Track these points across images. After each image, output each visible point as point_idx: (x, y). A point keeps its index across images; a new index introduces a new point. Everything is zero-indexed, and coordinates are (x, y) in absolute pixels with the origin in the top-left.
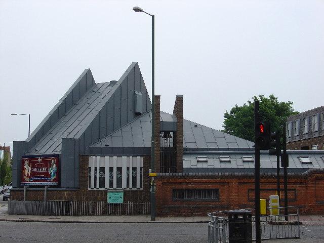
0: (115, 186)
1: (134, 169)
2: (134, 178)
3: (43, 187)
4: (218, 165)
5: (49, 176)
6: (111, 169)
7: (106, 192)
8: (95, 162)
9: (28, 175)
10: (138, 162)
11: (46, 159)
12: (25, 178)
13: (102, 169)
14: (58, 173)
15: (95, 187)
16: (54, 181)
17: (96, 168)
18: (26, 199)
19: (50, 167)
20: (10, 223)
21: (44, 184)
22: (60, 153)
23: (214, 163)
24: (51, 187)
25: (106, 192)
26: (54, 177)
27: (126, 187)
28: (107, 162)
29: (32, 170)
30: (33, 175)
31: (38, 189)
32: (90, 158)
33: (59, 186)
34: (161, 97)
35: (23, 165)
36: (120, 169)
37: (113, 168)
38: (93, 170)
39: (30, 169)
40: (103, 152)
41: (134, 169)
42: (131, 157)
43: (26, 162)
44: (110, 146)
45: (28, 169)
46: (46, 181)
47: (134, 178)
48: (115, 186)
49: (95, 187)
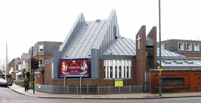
0: (118, 77)
1: (128, 67)
2: (128, 73)
3: (79, 77)
4: (176, 65)
5: (82, 71)
6: (116, 67)
7: (114, 80)
8: (108, 63)
9: (65, 71)
10: (129, 63)
11: (79, 62)
12: (63, 72)
13: (111, 67)
14: (89, 70)
15: (108, 78)
16: (85, 74)
17: (124, 67)
18: (159, 87)
19: (82, 66)
20: (195, 98)
21: (79, 76)
22: (90, 57)
23: (173, 64)
24: (83, 77)
25: (114, 80)
26: (86, 72)
27: (115, 78)
28: (114, 63)
29: (68, 68)
30: (68, 70)
31: (72, 79)
32: (104, 61)
33: (90, 77)
34: (84, 15)
35: (61, 65)
36: (120, 67)
37: (118, 68)
38: (106, 68)
39: (67, 67)
40: (112, 57)
41: (128, 67)
42: (126, 61)
43: (64, 63)
44: (112, 54)
45: (64, 67)
46: (79, 74)
47: (128, 73)
48: (118, 77)
49: (108, 78)
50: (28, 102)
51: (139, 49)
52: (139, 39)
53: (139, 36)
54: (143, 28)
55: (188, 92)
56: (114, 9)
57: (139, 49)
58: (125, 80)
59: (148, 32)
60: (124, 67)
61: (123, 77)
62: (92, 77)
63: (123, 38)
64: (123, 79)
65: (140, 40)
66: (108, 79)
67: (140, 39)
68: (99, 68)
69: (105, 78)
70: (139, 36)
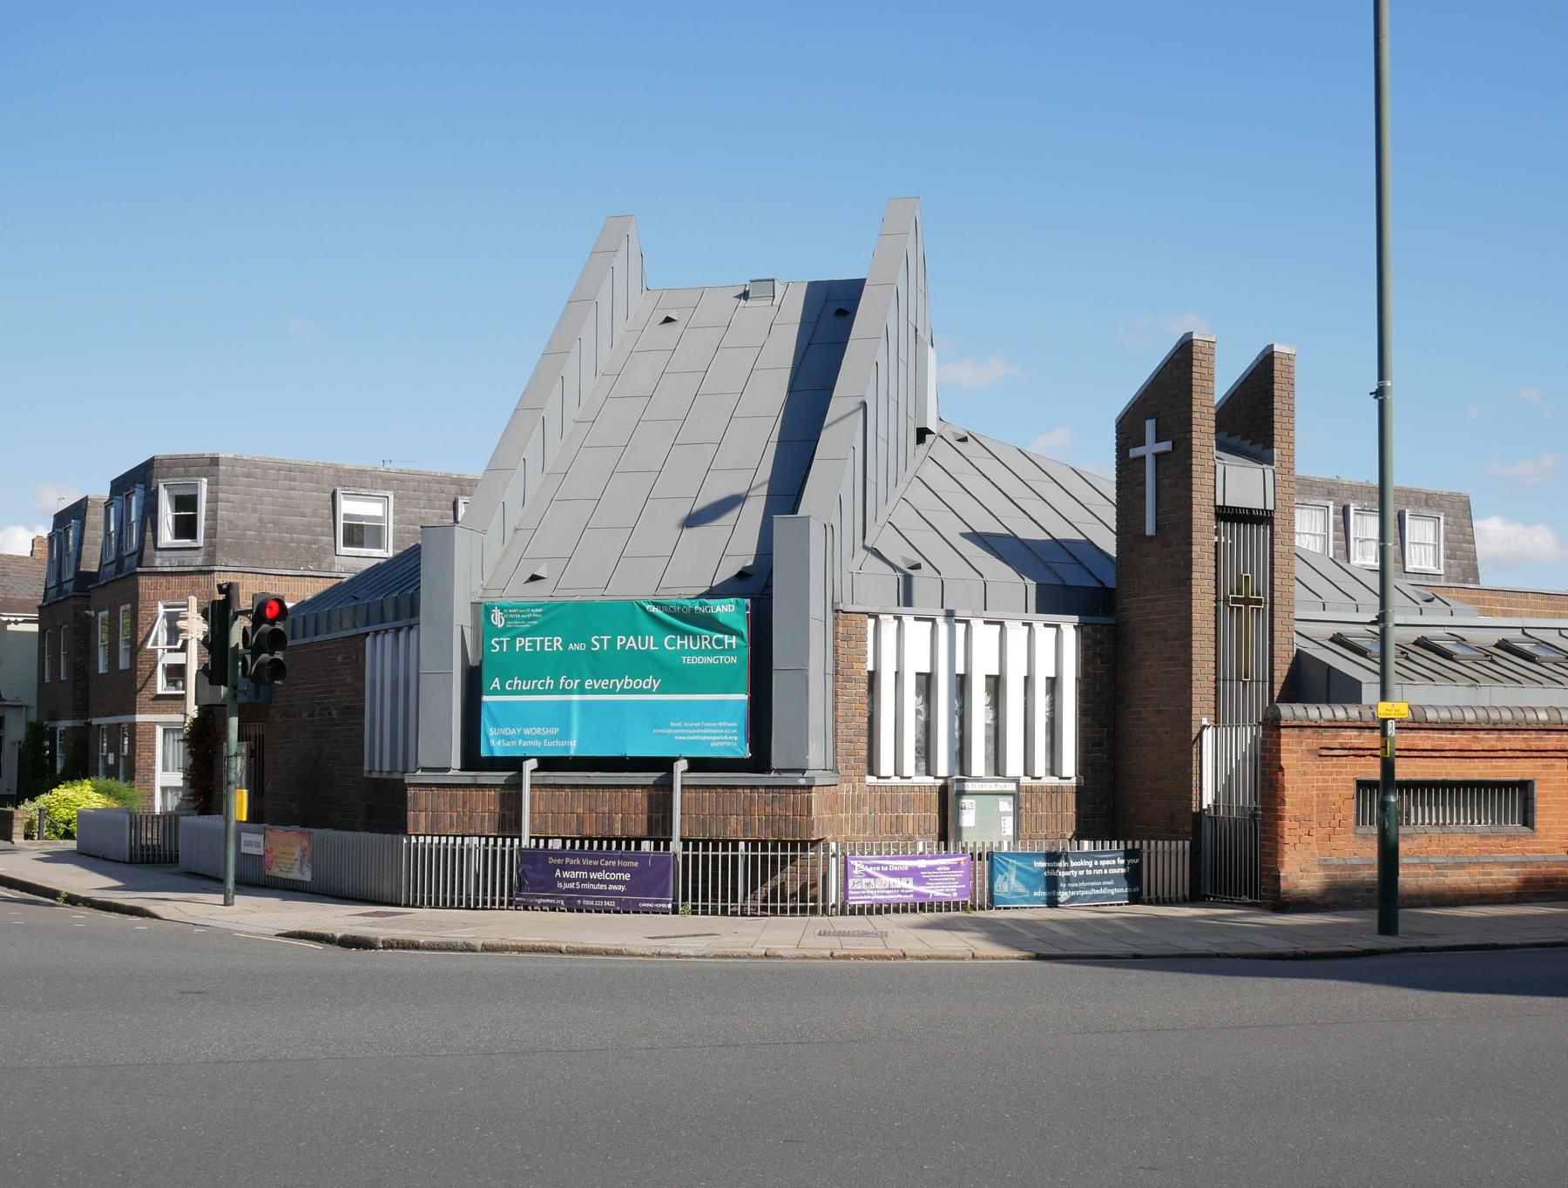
15: (898, 771)
50: (6, 744)
51: (1150, 530)
52: (1150, 448)
53: (1150, 426)
54: (1181, 363)
55: (1546, 880)
56: (1464, 491)
57: (1150, 530)
58: (1030, 790)
59: (1221, 377)
60: (1028, 681)
61: (1014, 766)
62: (776, 762)
63: (964, 440)
64: (1016, 780)
65: (1157, 456)
66: (896, 780)
67: (1166, 446)
68: (830, 679)
69: (872, 767)
70: (1150, 426)
